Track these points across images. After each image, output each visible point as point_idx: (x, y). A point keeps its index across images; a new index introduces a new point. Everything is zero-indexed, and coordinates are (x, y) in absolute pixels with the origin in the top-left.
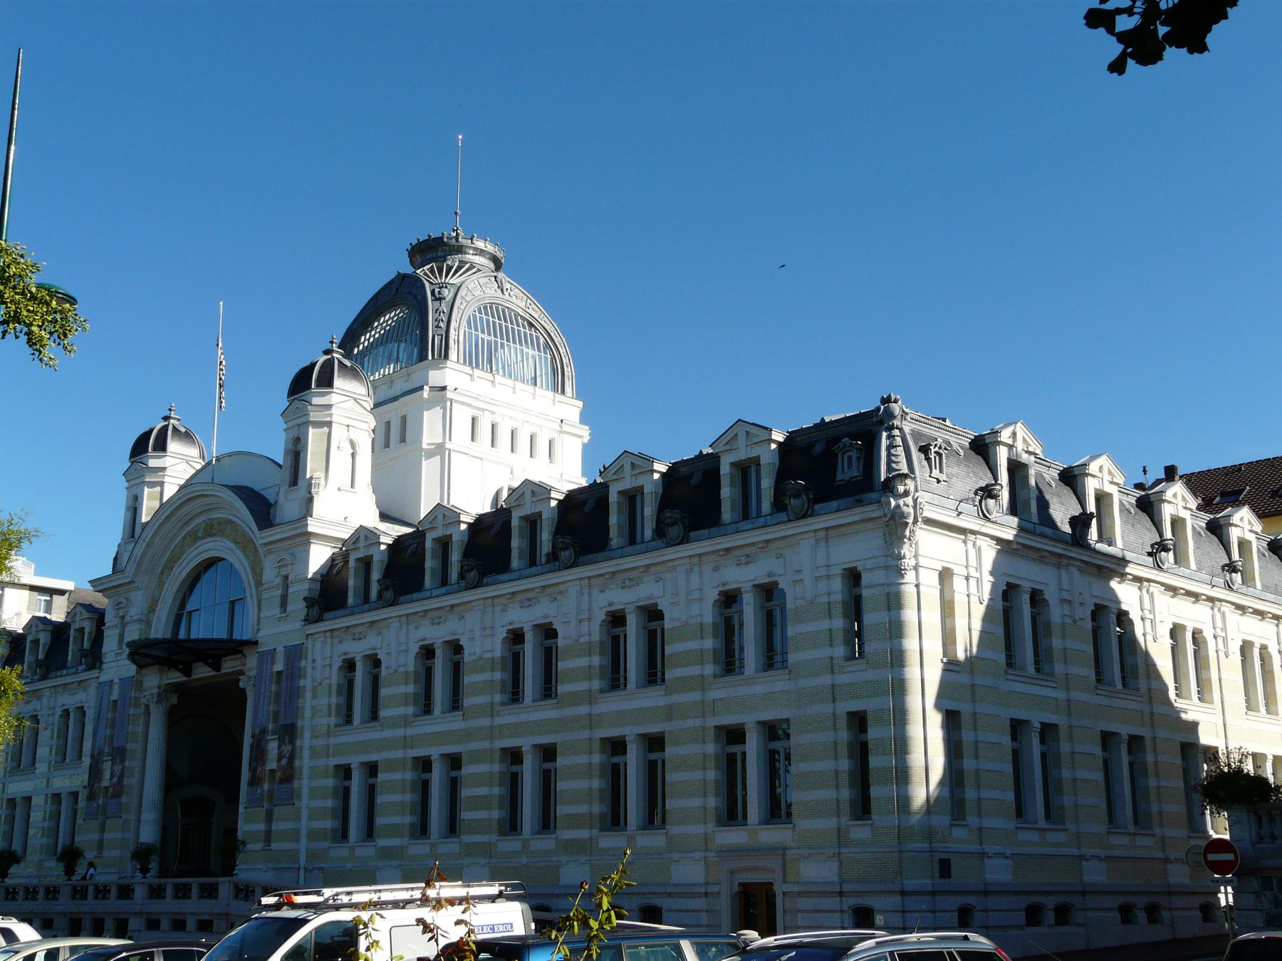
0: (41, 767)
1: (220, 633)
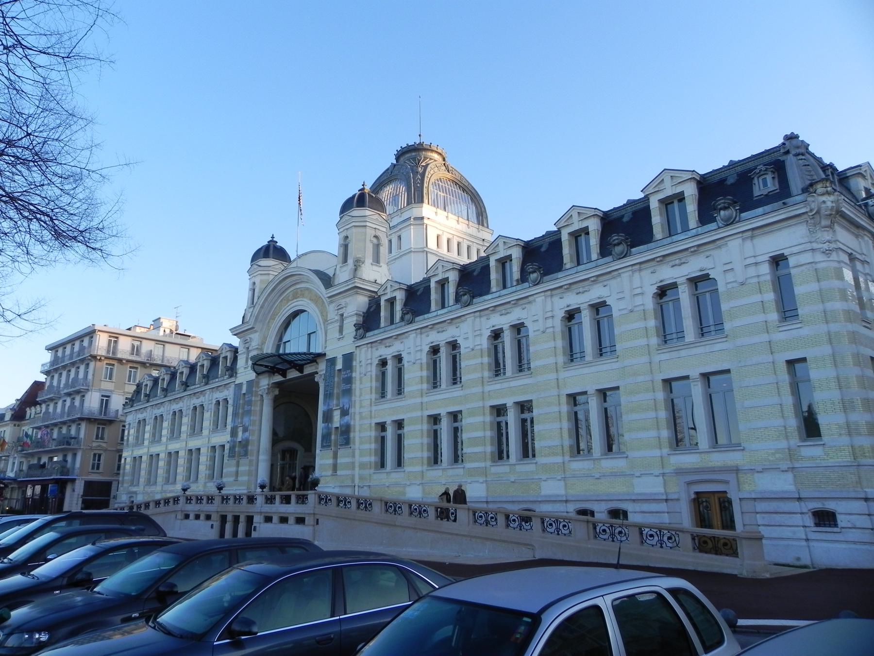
0: (205, 432)
1: (303, 349)
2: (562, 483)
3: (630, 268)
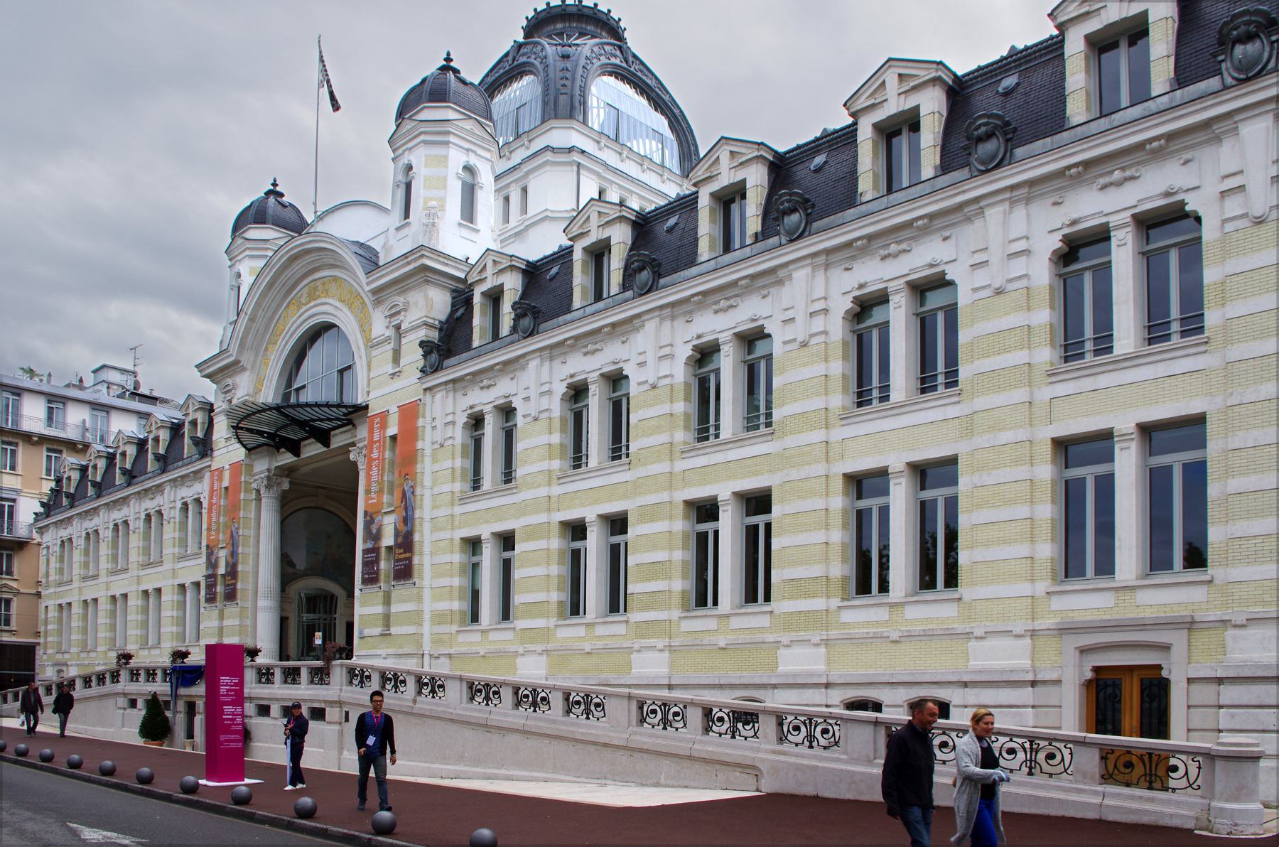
2: (822, 650)
3: (1007, 195)
